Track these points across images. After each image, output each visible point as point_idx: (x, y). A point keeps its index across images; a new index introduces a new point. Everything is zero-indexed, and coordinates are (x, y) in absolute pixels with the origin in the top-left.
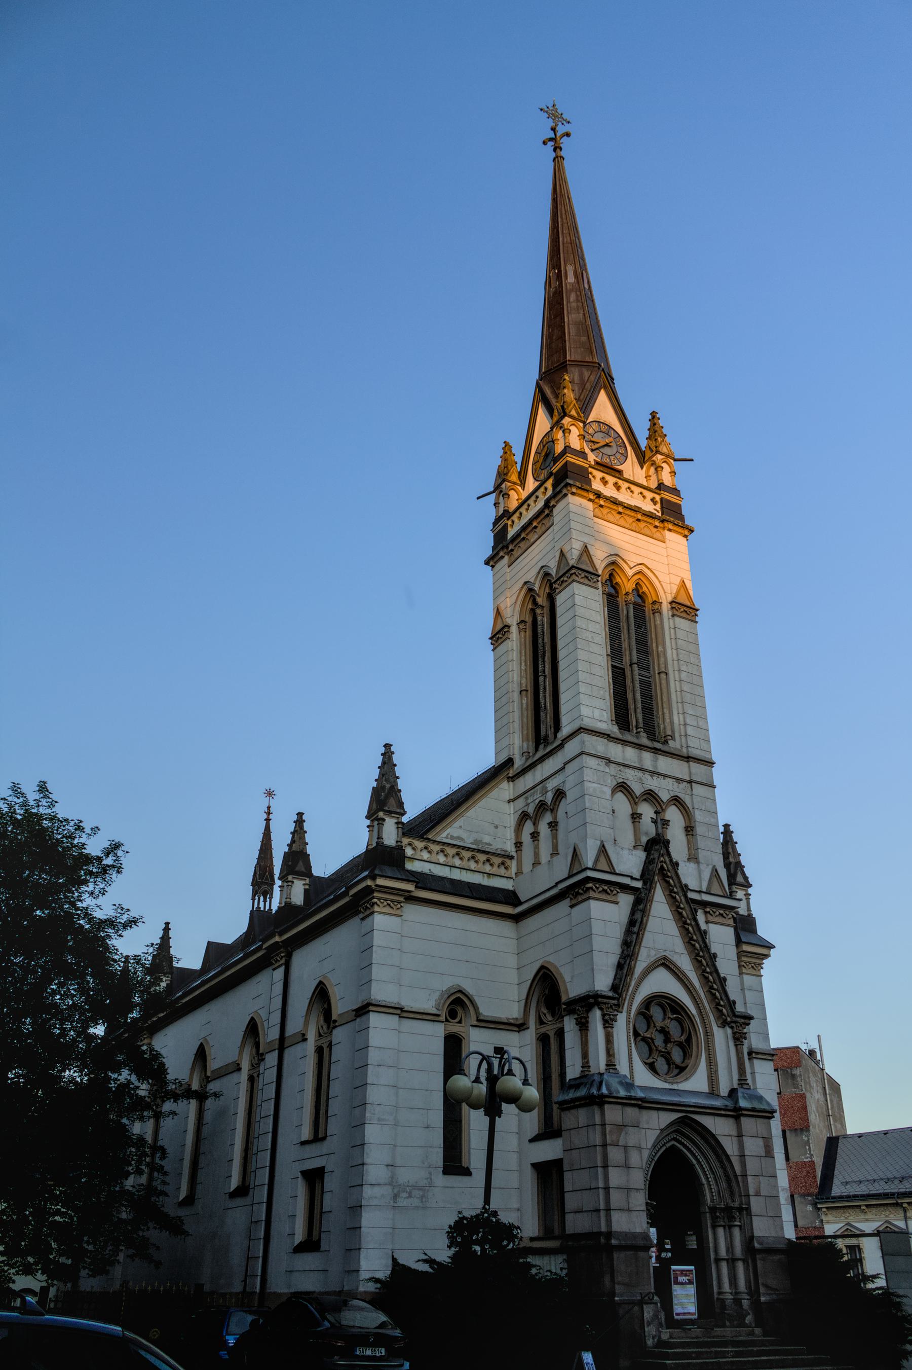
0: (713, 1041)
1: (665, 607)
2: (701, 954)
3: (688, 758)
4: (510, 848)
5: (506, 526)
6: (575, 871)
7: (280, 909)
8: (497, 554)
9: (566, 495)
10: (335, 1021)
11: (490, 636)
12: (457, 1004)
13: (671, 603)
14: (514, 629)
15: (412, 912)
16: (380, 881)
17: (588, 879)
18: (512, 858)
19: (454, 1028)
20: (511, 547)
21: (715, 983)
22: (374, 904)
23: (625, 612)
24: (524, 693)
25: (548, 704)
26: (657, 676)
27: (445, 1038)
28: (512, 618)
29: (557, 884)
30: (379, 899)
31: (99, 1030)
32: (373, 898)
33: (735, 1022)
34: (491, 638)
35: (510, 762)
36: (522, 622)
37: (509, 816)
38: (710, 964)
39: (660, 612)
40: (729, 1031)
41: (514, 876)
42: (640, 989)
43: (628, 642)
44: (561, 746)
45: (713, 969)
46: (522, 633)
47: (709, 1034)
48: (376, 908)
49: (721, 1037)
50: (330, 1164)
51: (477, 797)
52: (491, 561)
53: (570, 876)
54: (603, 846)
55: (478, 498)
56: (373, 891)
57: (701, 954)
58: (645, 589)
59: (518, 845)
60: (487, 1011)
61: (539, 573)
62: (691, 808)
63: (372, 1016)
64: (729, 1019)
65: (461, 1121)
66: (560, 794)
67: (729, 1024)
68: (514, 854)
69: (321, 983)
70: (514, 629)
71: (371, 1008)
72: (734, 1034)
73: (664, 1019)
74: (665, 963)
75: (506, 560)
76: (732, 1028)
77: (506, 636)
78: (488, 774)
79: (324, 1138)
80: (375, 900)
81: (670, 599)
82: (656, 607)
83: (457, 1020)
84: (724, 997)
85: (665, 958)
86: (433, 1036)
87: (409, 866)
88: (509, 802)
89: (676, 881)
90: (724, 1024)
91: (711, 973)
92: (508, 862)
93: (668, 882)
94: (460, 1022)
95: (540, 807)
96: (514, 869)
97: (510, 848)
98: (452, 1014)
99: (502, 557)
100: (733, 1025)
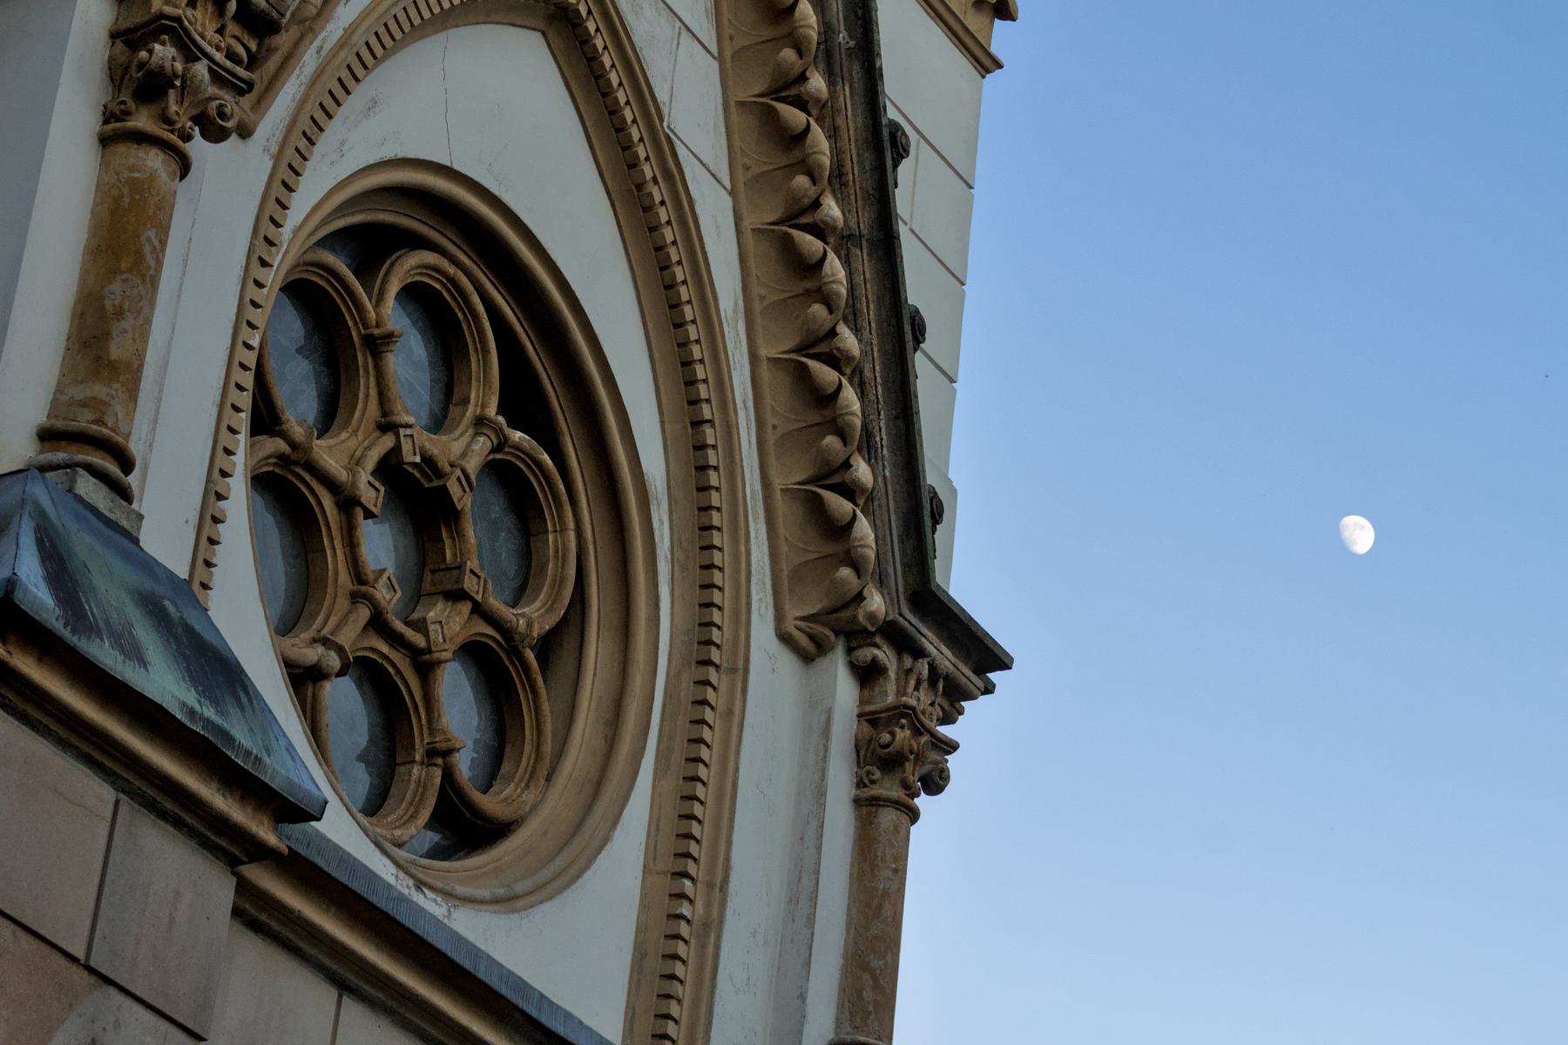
0: (734, 717)
2: (817, 83)
7: (166, 94)
31: (1360, 534)
33: (905, 645)
38: (853, 172)
40: (844, 691)
42: (334, 131)
45: (864, 222)
47: (709, 656)
49: (790, 716)
50: (257, 81)
57: (817, 83)
64: (876, 602)
67: (855, 636)
72: (871, 719)
73: (438, 424)
76: (867, 675)
78: (208, 636)
84: (883, 437)
90: (829, 630)
91: (844, 242)
100: (884, 654)
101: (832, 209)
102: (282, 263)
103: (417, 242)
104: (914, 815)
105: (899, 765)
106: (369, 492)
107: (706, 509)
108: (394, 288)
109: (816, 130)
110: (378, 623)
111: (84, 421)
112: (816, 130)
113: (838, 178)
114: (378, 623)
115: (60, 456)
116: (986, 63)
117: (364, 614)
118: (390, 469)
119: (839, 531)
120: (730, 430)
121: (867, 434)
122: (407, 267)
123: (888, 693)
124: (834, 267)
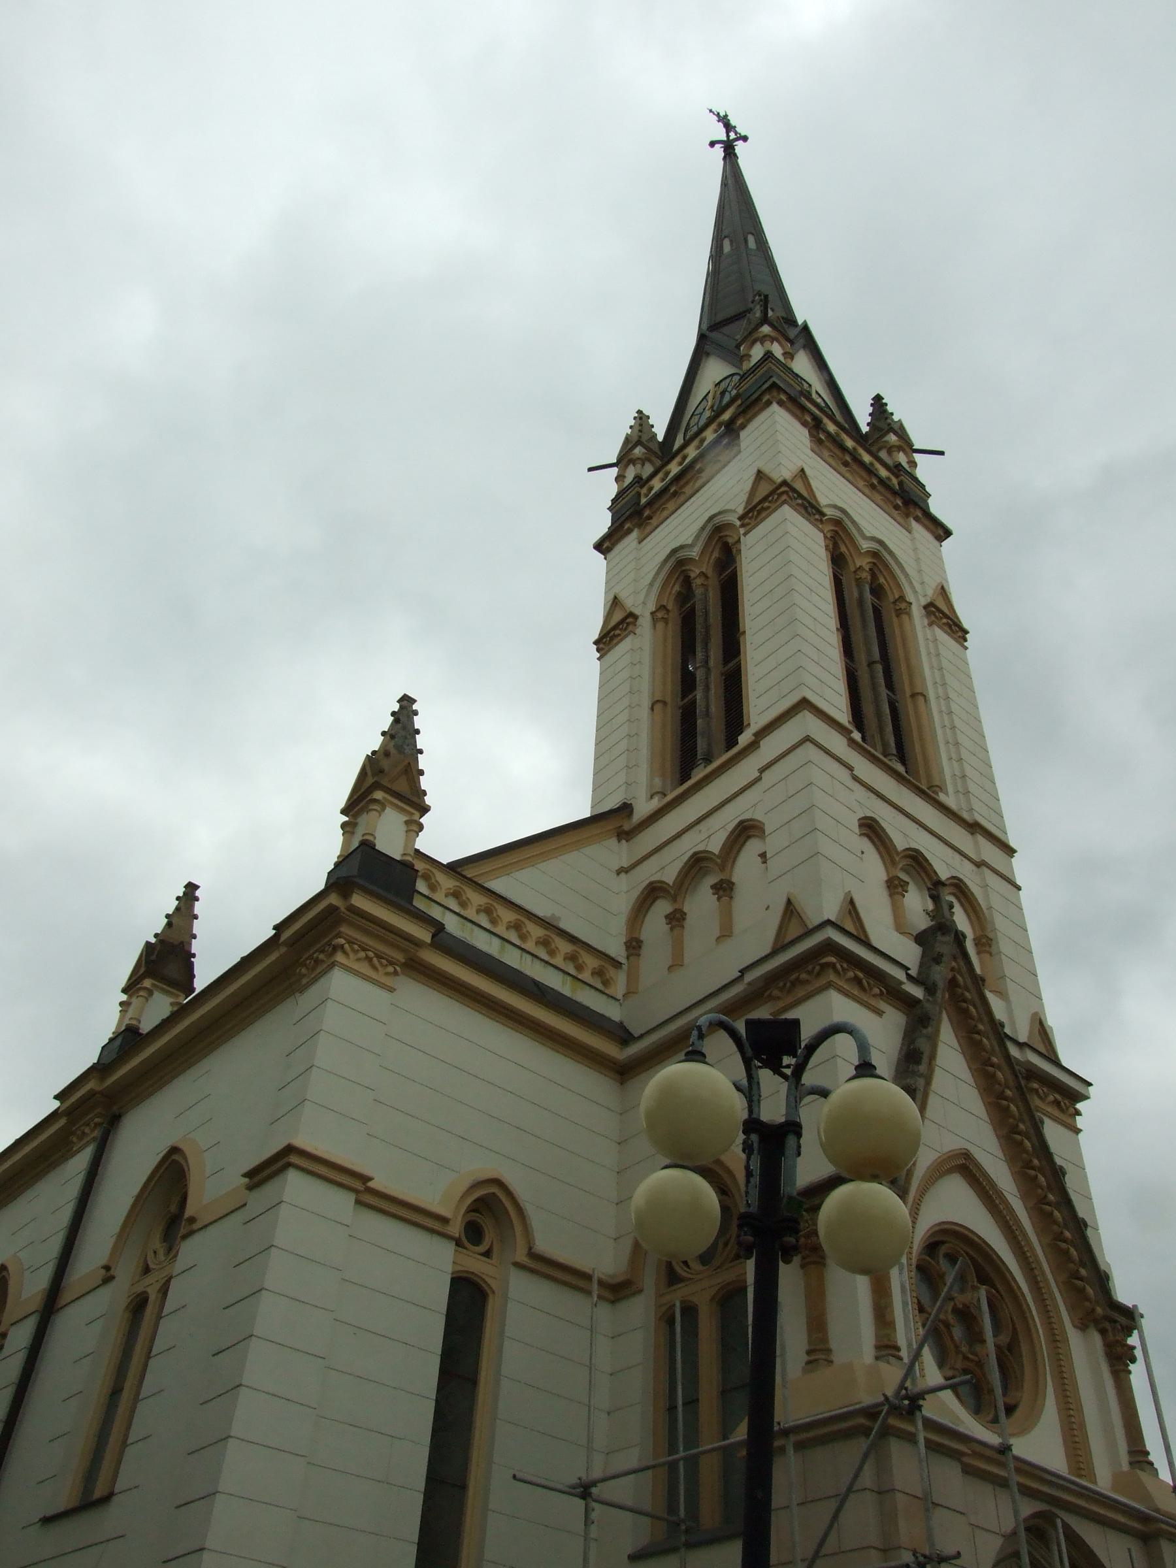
1: (917, 612)
3: (974, 827)
4: (616, 948)
5: (639, 494)
6: (788, 939)
8: (622, 525)
9: (769, 403)
10: (192, 1220)
11: (596, 637)
12: (488, 1214)
13: (925, 607)
14: (645, 622)
15: (415, 996)
16: (359, 900)
17: (829, 947)
18: (617, 964)
19: (474, 1264)
20: (647, 513)
21: (1066, 1227)
22: (335, 948)
23: (856, 594)
24: (658, 707)
25: (713, 709)
26: (909, 701)
27: (453, 1279)
28: (642, 603)
29: (743, 972)
30: (350, 942)
32: (339, 935)
34: (596, 643)
35: (625, 809)
36: (662, 607)
37: (622, 896)
39: (909, 614)
41: (619, 996)
43: (864, 637)
44: (754, 745)
46: (660, 625)
47: (1057, 1340)
48: (339, 957)
49: (1084, 1351)
51: (757, 409)
52: (603, 546)
53: (779, 947)
54: (852, 902)
55: (590, 469)
56: (340, 921)
57: (1036, 1162)
58: (882, 580)
59: (634, 946)
60: (545, 1244)
61: (703, 528)
62: (984, 906)
63: (292, 1176)
64: (1099, 1310)
65: (464, 1487)
66: (746, 831)
67: (1096, 1322)
68: (623, 961)
69: (174, 1150)
70: (645, 622)
71: (294, 1159)
74: (965, 1166)
75: (635, 534)
77: (630, 628)
79: (107, 1499)
80: (342, 941)
81: (924, 602)
82: (903, 606)
83: (483, 1248)
85: (967, 1155)
86: (432, 1266)
87: (419, 903)
88: (619, 872)
89: (981, 1010)
91: (1057, 1206)
92: (611, 972)
93: (966, 1012)
94: (487, 1254)
95: (692, 866)
96: (619, 989)
97: (616, 948)
98: (473, 1233)
99: (629, 531)
100: (1107, 1325)
101: (1051, 1197)
102: (914, 1262)
103: (943, 1242)
104: (1130, 1372)
105: (1119, 1358)
106: (951, 1318)
107: (1050, 1317)
108: (941, 1256)
109: (1040, 1176)
110: (965, 1358)
111: (886, 1342)
112: (1040, 1176)
113: (1049, 1188)
114: (965, 1358)
115: (884, 1353)
116: (966, 648)
117: (961, 1356)
118: (955, 1311)
119: (1082, 1291)
120: (1046, 1280)
121: (1081, 1261)
122: (943, 1250)
123: (1111, 1337)
124: (1056, 1213)
